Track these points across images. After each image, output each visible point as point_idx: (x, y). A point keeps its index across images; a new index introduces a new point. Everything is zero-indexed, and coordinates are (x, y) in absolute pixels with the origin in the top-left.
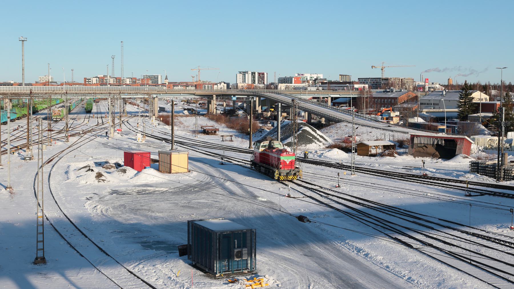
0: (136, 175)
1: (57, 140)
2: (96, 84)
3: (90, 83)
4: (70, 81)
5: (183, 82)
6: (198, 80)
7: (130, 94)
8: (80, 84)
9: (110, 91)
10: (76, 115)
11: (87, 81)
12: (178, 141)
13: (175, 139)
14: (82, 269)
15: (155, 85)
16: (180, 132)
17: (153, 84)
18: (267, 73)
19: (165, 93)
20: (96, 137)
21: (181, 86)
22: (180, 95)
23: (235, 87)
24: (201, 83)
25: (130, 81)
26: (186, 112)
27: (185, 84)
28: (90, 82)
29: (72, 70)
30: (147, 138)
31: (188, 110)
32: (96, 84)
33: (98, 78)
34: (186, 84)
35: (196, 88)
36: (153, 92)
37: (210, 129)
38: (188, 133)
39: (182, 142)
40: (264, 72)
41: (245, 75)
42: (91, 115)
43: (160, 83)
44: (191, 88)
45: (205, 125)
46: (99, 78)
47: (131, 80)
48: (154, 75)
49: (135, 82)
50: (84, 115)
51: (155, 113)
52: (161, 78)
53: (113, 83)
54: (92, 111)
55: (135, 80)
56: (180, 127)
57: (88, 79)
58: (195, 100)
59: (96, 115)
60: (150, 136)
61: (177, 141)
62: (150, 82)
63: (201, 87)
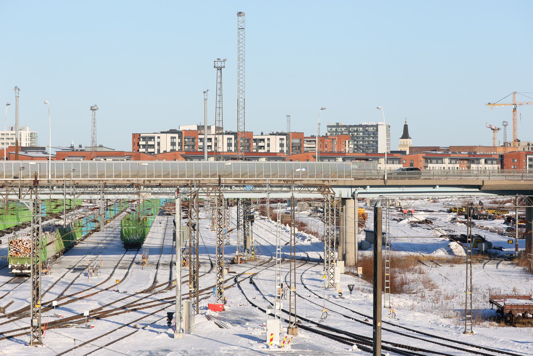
1: (8, 338)
2: (172, 155)
3: (150, 150)
4: (87, 144)
5: (459, 147)
6: (510, 139)
7: (259, 186)
8: (119, 154)
9: (151, 176)
10: (88, 256)
11: (142, 143)
12: (403, 346)
13: (385, 336)
15: (363, 155)
16: (417, 314)
17: (361, 154)
19: (382, 183)
20: (135, 330)
21: (451, 159)
22: (431, 189)
24: (520, 149)
25: (282, 145)
26: (457, 248)
27: (465, 154)
28: (153, 146)
29: (92, 109)
30: (302, 335)
31: (463, 240)
32: (172, 155)
33: (176, 135)
34: (469, 154)
35: (502, 167)
36: (341, 181)
37: (517, 306)
38: (446, 321)
39: (416, 349)
42: (139, 257)
43: (382, 148)
44: (487, 166)
45: (510, 292)
46: (180, 133)
47: (284, 142)
49: (299, 147)
50: (117, 257)
51: (349, 249)
52: (388, 135)
53: (225, 150)
54: (148, 243)
55: (297, 141)
56: (423, 297)
57: (144, 138)
58: (496, 206)
59: (153, 258)
60: (314, 327)
61: (400, 346)
62: (349, 147)
63: (519, 161)
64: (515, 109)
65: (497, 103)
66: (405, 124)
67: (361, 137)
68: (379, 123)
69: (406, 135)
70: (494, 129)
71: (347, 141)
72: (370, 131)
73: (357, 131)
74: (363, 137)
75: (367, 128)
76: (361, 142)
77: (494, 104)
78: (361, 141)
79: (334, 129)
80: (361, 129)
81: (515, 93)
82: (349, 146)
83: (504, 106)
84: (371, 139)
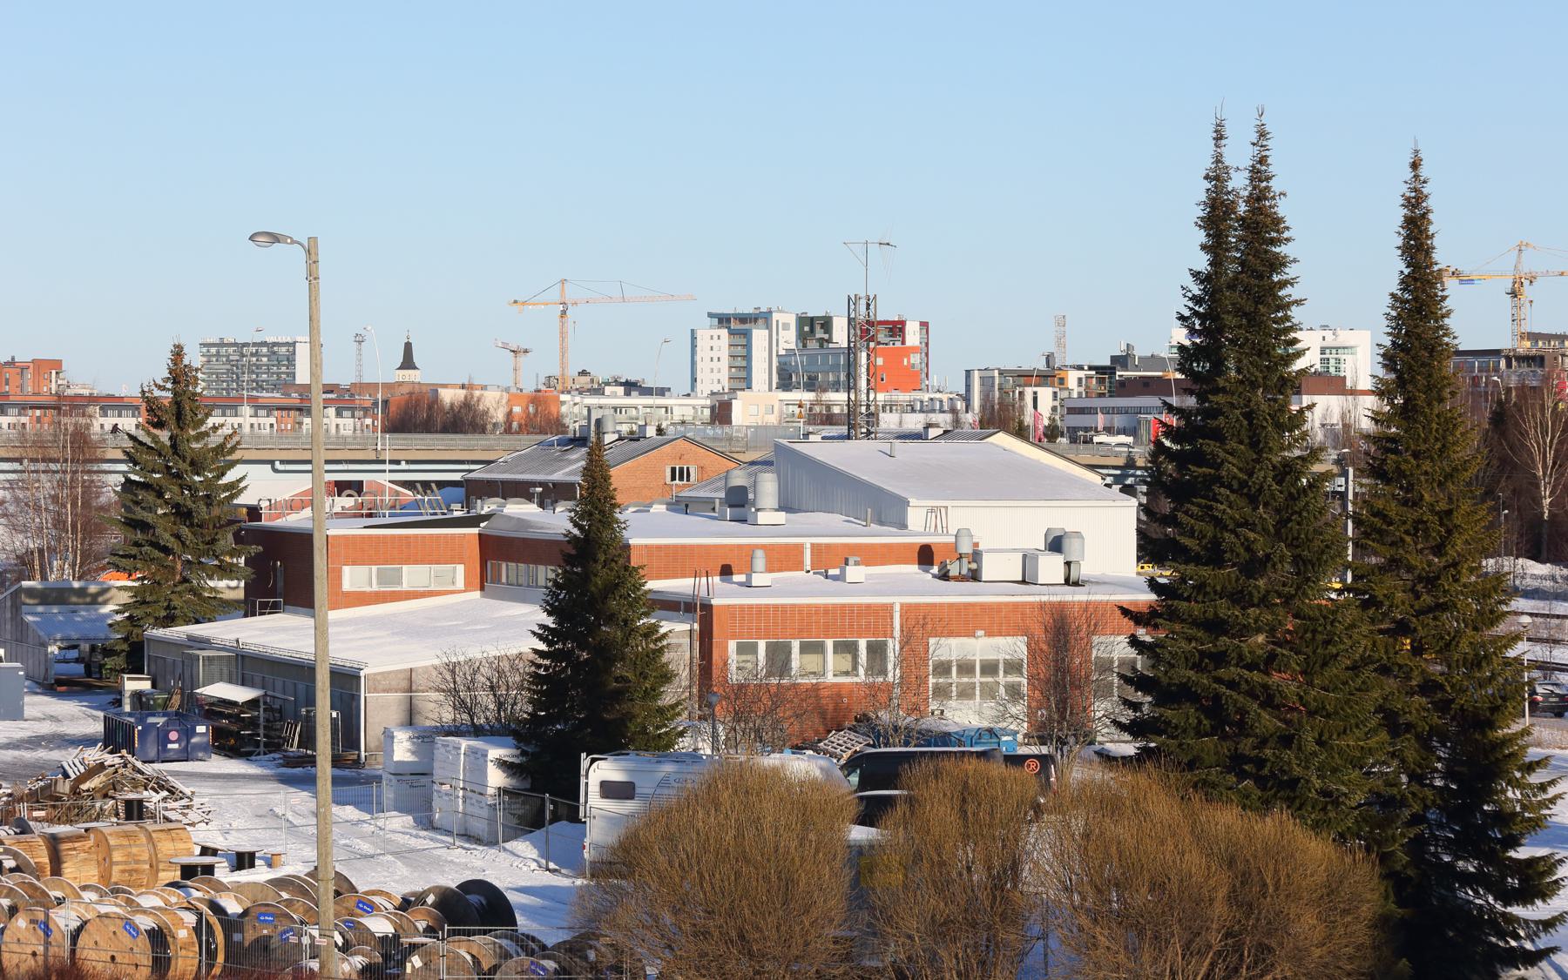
0: (445, 386)
14: (403, 403)
18: (924, 325)
21: (257, 408)
23: (894, 408)
40: (831, 315)
41: (747, 335)
48: (270, 339)
64: (564, 313)
65: (531, 302)
68: (298, 339)
69: (408, 363)
74: (268, 365)
76: (265, 376)
77: (524, 303)
78: (265, 373)
79: (213, 350)
80: (265, 350)
81: (563, 281)
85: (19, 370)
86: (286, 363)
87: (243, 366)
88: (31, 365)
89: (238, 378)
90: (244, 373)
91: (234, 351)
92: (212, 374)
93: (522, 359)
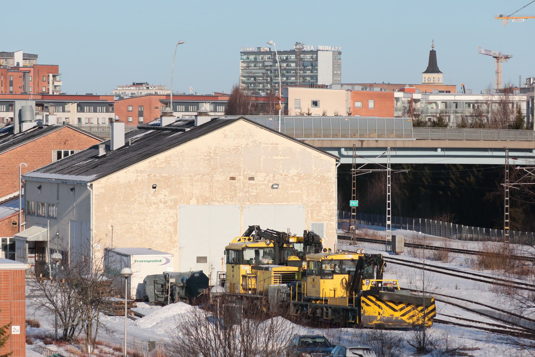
66: (431, 49)
67: (293, 70)
68: (320, 48)
69: (433, 68)
70: (498, 57)
71: (51, 75)
72: (306, 60)
73: (286, 61)
74: (295, 70)
75: (302, 56)
76: (293, 79)
77: (508, 17)
79: (252, 57)
80: (293, 57)
82: (53, 83)
83: (524, 20)
84: (308, 73)
85: (22, 74)
86: (310, 67)
87: (275, 70)
88: (32, 69)
89: (271, 80)
90: (277, 76)
91: (269, 58)
92: (251, 77)
93: (503, 63)
